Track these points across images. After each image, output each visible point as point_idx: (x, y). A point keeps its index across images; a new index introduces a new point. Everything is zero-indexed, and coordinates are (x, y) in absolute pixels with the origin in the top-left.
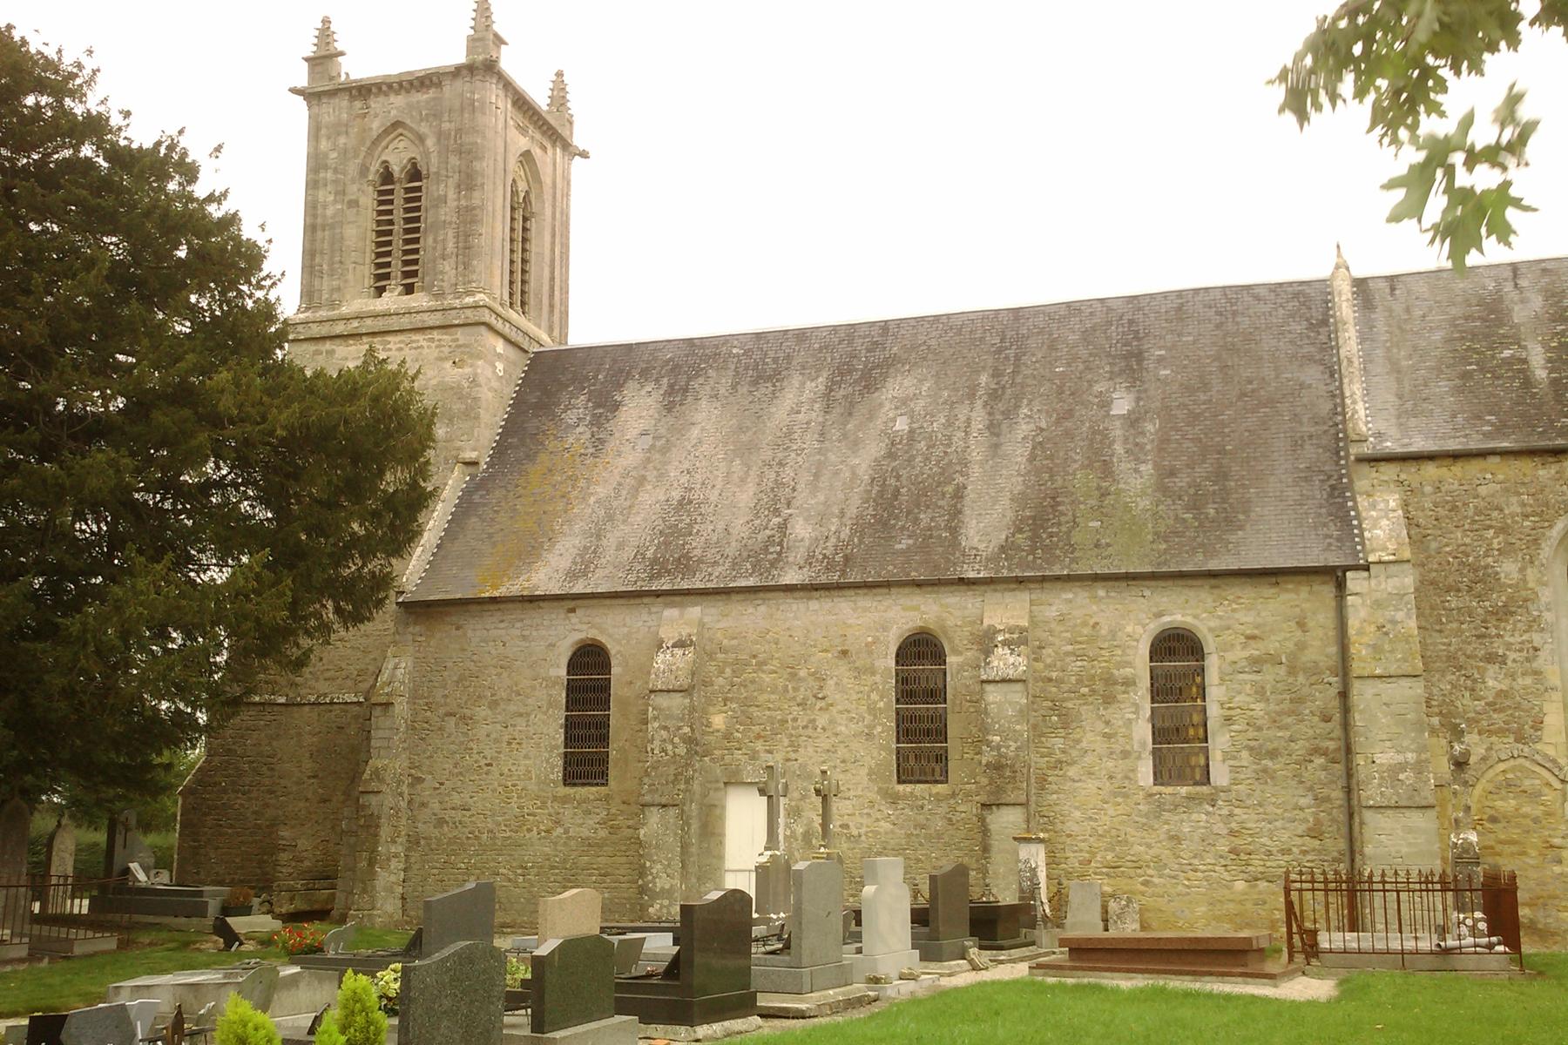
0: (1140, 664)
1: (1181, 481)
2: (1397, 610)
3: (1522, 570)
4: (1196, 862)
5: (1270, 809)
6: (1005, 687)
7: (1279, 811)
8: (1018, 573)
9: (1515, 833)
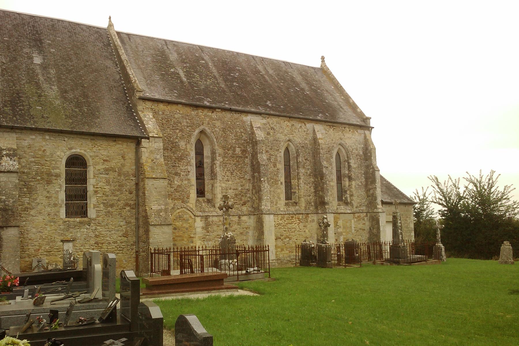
0: (62, 169)
1: (70, 95)
2: (157, 155)
3: (186, 145)
4: (82, 248)
5: (110, 226)
6: (9, 175)
7: (113, 227)
8: (10, 124)
9: (181, 233)
